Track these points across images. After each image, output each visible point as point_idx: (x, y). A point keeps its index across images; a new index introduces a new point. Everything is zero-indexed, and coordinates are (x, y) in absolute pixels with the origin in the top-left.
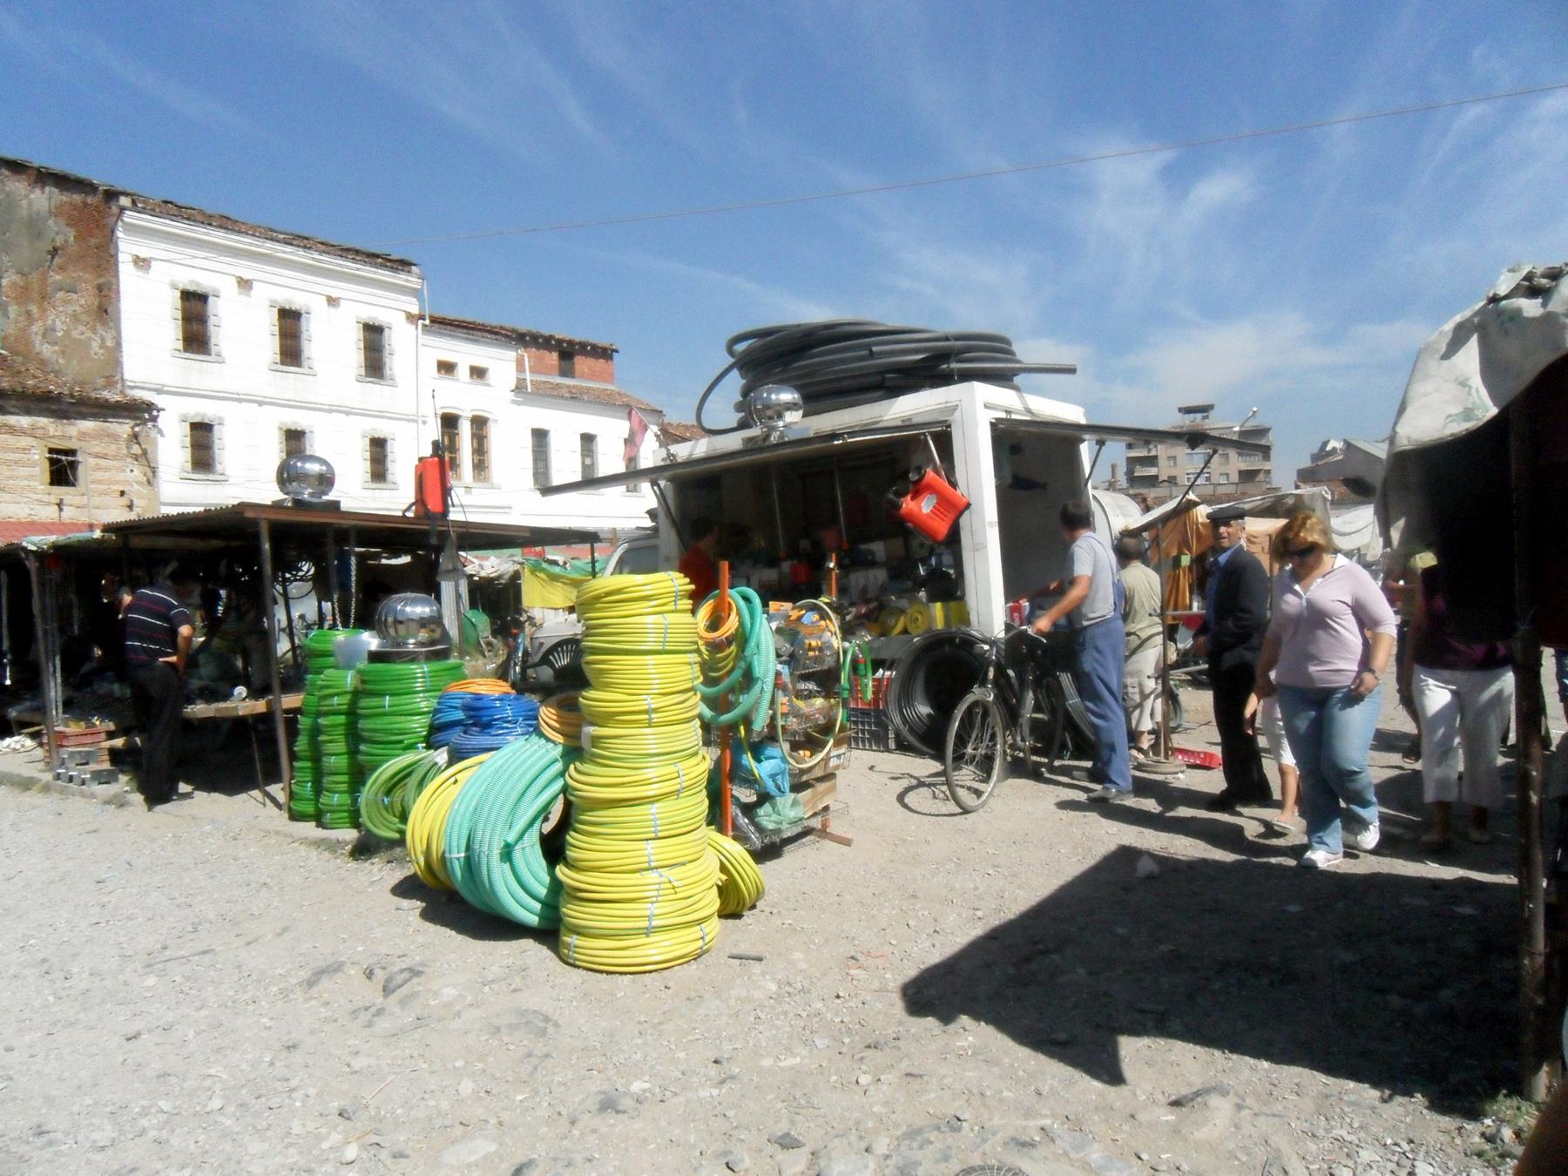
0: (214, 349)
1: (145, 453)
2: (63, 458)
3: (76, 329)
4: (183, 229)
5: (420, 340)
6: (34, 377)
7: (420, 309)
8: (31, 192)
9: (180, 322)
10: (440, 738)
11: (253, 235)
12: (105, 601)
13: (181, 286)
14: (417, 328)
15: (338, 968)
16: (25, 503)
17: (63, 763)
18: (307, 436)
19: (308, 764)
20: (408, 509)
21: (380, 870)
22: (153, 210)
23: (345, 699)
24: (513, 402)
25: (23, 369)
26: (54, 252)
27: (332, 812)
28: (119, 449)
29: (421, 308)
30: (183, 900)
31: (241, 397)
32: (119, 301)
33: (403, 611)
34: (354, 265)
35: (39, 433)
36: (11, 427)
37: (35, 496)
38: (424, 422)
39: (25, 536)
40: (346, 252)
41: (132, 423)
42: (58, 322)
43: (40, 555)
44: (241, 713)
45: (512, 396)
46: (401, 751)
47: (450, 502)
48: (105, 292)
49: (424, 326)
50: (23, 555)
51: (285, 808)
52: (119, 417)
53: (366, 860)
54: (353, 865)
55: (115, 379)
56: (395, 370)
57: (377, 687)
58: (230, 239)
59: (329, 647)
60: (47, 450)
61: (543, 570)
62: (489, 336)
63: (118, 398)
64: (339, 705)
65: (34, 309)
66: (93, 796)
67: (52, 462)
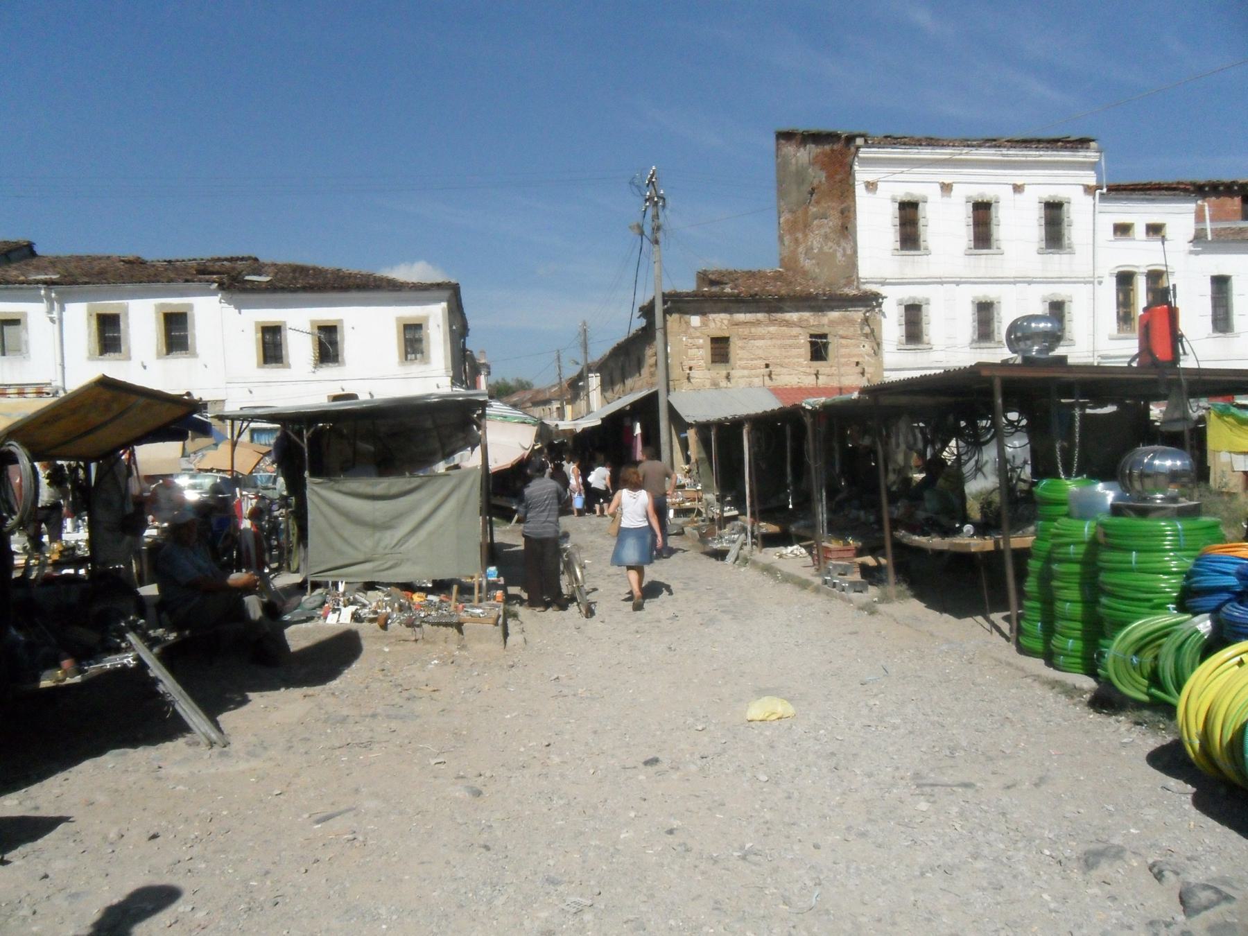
0: (922, 244)
1: (872, 331)
2: (819, 341)
3: (826, 245)
4: (900, 153)
5: (1097, 207)
6: (801, 284)
7: (1097, 181)
8: (798, 151)
9: (898, 228)
10: (1197, 604)
11: (953, 146)
12: (850, 445)
13: (899, 199)
14: (1094, 198)
15: (1118, 853)
16: (796, 374)
17: (829, 573)
18: (995, 306)
19: (1037, 605)
20: (1133, 359)
21: (1128, 730)
22: (879, 143)
23: (1082, 549)
24: (1191, 252)
25: (793, 280)
26: (812, 192)
27: (1066, 655)
28: (855, 331)
29: (1099, 178)
30: (936, 718)
31: (944, 280)
32: (855, 219)
33: (1150, 465)
34: (1037, 153)
35: (804, 324)
36: (787, 321)
37: (802, 369)
38: (1100, 283)
39: (803, 398)
40: (1026, 143)
41: (863, 310)
42: (815, 242)
43: (814, 413)
44: (973, 550)
45: (1190, 247)
46: (1147, 610)
47: (1181, 351)
48: (846, 214)
49: (1102, 194)
50: (802, 413)
51: (1013, 640)
52: (855, 306)
53: (1109, 715)
54: (1093, 716)
55: (852, 278)
56: (1072, 239)
57: (1125, 542)
58: (937, 153)
59: (1063, 496)
60: (808, 336)
61: (1232, 415)
62: (1166, 193)
63: (855, 292)
64: (1074, 554)
65: (800, 235)
66: (850, 601)
67: (813, 344)
